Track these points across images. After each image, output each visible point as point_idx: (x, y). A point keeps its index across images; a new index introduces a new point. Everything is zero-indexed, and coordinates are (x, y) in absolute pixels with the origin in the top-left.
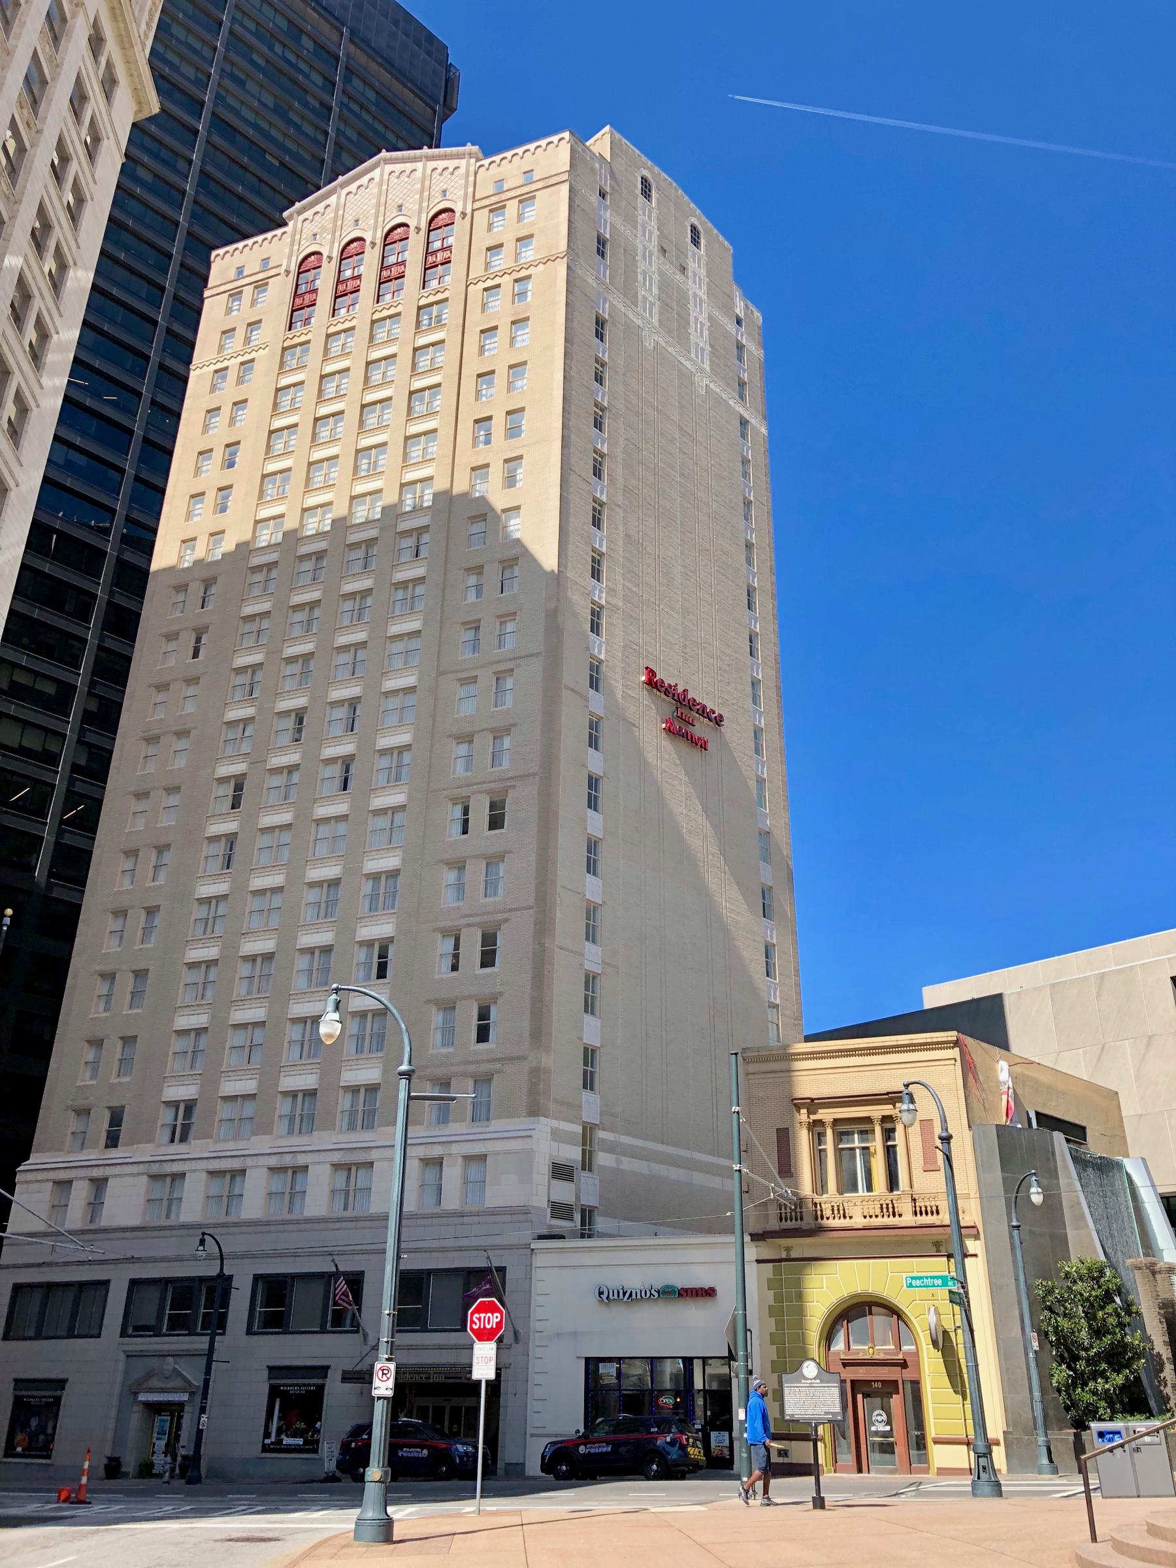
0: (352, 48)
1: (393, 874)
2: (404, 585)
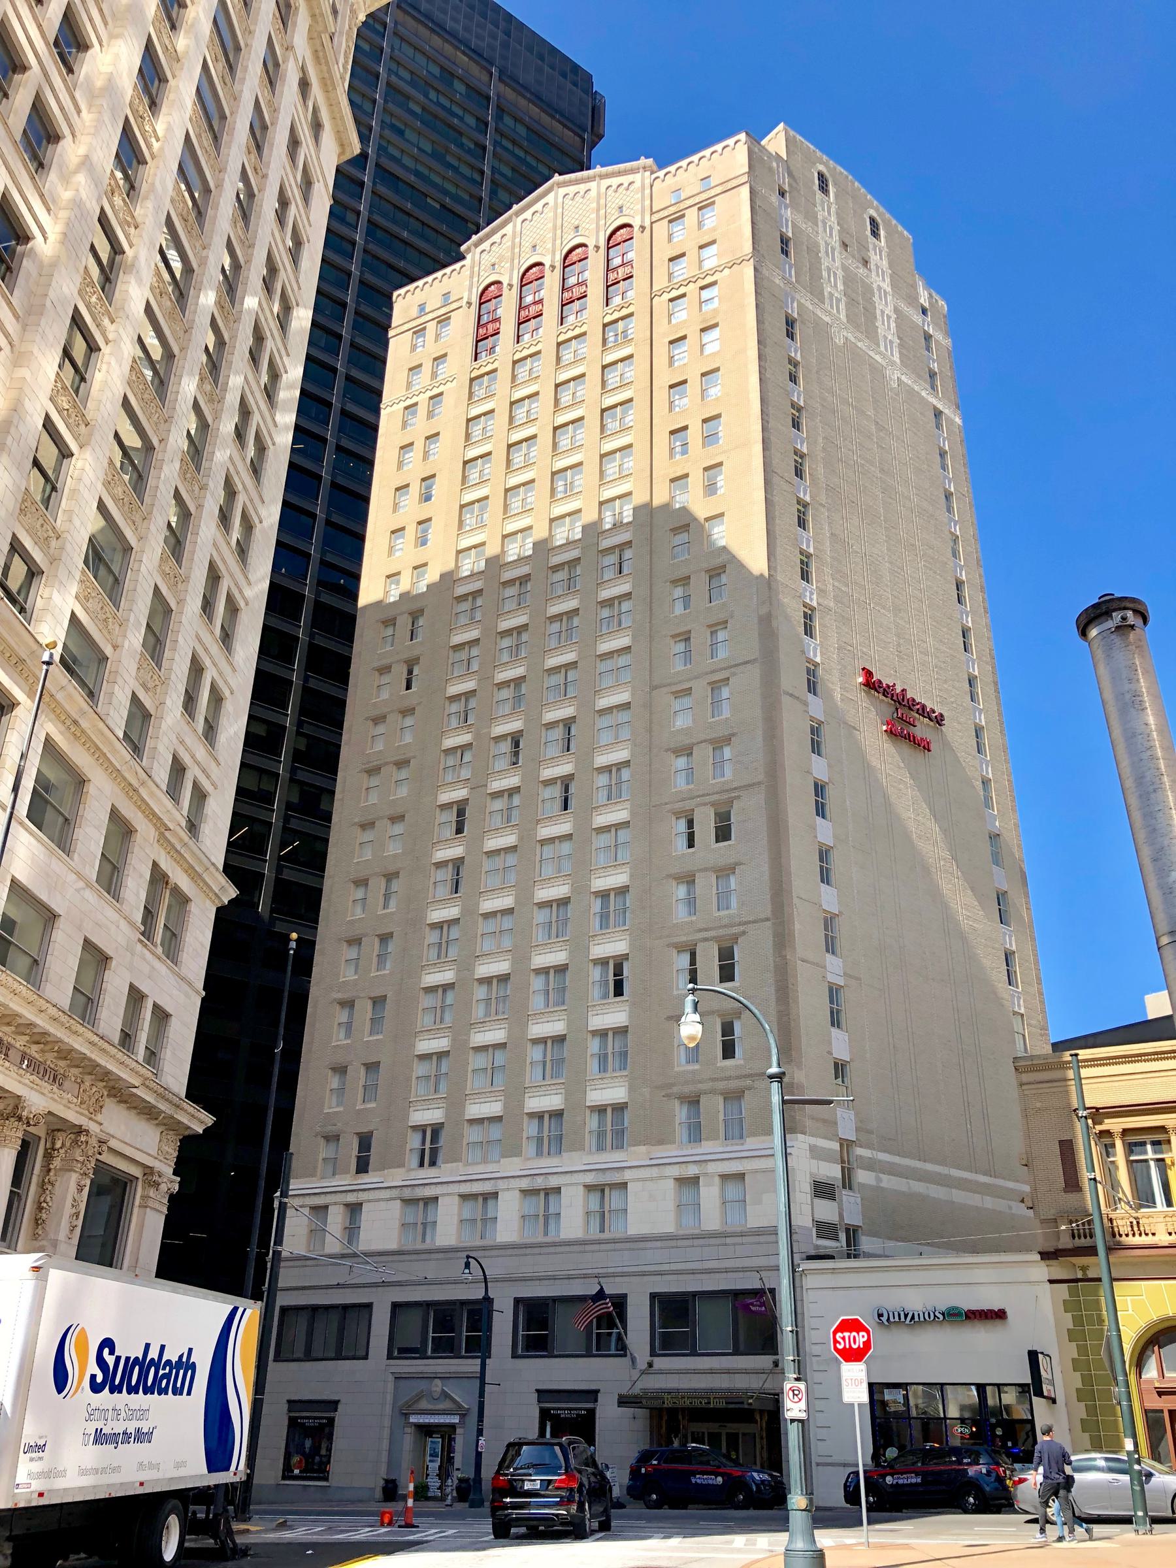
0: (501, 87)
1: (623, 891)
2: (608, 603)
